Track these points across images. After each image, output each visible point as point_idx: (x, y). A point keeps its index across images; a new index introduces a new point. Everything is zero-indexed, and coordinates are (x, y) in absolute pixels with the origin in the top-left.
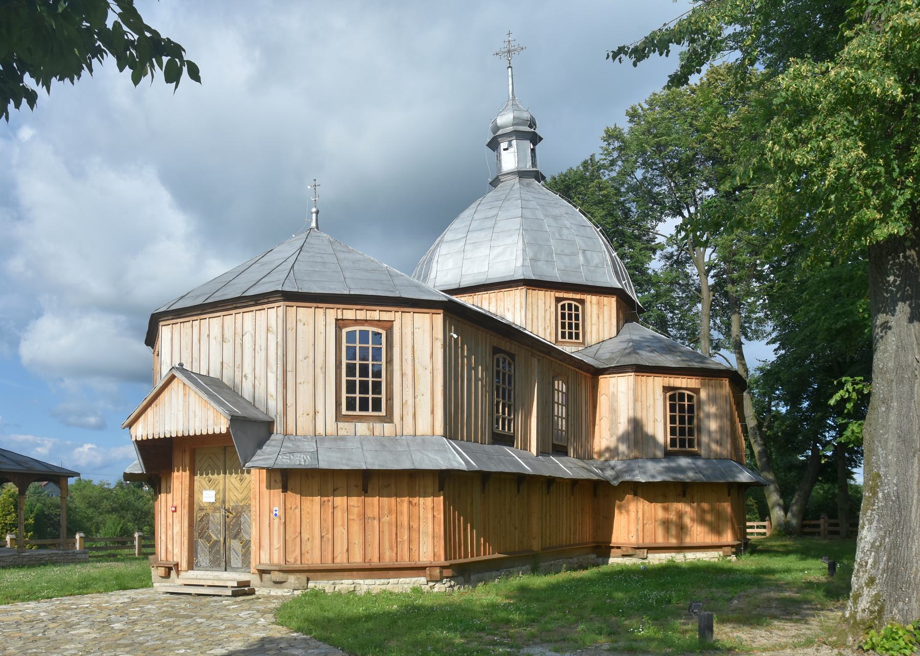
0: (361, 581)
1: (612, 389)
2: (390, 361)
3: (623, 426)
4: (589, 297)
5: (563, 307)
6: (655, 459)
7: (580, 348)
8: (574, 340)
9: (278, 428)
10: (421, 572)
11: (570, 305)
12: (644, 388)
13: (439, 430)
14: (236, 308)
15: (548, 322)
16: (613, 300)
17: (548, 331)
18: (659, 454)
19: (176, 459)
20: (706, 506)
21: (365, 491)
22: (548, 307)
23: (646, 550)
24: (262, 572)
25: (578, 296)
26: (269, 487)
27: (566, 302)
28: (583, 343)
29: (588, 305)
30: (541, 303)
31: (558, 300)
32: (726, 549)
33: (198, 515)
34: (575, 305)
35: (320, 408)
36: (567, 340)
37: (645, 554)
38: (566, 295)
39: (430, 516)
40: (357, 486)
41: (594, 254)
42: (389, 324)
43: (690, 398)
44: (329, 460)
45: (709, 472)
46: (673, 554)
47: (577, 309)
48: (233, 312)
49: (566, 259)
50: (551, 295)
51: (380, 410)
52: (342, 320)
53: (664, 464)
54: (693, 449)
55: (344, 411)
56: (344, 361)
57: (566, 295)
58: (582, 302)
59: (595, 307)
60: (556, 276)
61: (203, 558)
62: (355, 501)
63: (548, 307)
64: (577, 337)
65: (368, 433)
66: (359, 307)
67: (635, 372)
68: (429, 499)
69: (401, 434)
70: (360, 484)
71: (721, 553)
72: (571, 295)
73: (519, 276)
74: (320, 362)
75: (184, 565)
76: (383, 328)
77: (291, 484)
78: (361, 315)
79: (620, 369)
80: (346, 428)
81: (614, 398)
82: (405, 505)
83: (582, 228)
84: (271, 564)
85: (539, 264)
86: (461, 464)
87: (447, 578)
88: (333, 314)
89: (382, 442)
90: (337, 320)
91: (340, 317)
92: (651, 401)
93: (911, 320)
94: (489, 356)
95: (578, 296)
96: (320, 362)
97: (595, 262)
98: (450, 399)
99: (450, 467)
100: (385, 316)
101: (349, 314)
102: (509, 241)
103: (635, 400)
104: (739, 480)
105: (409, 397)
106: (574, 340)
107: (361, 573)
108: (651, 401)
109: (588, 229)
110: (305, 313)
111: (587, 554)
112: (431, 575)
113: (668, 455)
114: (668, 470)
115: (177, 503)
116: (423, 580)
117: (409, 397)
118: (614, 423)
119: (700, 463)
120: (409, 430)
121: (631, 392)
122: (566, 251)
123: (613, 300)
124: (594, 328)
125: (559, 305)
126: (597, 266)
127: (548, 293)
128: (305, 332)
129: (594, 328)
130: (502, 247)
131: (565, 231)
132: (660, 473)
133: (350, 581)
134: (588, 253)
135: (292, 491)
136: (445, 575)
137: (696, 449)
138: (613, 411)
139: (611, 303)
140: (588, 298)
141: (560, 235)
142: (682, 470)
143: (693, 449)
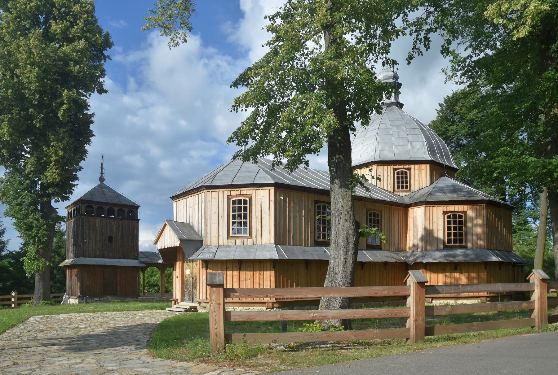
0: (237, 308)
1: (415, 214)
2: (251, 212)
3: (420, 232)
4: (413, 166)
5: (398, 173)
6: (438, 250)
7: (408, 194)
8: (404, 190)
9: (205, 243)
10: (264, 305)
11: (402, 173)
12: (431, 213)
13: (273, 241)
14: (193, 194)
15: (389, 181)
16: (428, 167)
17: (389, 186)
18: (442, 246)
19: (178, 257)
20: (473, 275)
21: (240, 269)
22: (389, 174)
23: (431, 299)
24: (200, 303)
25: (407, 167)
26: (202, 268)
27: (400, 170)
28: (410, 190)
29: (413, 170)
30: (385, 172)
31: (395, 170)
32: (483, 299)
33: (185, 279)
34: (405, 171)
35: (221, 234)
36: (400, 190)
37: (431, 300)
38: (400, 167)
39: (269, 279)
40: (236, 267)
41: (417, 143)
42: (251, 195)
43: (461, 217)
44: (221, 256)
45: (473, 256)
46: (448, 301)
47: (406, 173)
48: (192, 195)
49: (400, 148)
50: (391, 168)
51: (247, 234)
52: (230, 195)
53: (445, 253)
54: (462, 244)
55: (231, 235)
56: (231, 213)
57: (400, 167)
58: (409, 169)
59: (417, 172)
60: (390, 156)
61: (186, 297)
62: (235, 273)
63: (389, 174)
64: (406, 188)
65: (241, 244)
66: (237, 189)
67: (425, 205)
68: (268, 272)
69: (261, 243)
70: (238, 266)
71: (479, 301)
72: (402, 166)
73: (372, 160)
74: (221, 215)
75: (180, 300)
76: (248, 197)
77: (209, 266)
78: (238, 193)
79: (418, 204)
80: (232, 242)
81: (415, 219)
82: (258, 274)
83: (413, 130)
84: (203, 300)
85: (384, 152)
86: (277, 256)
87: (276, 307)
88: (226, 193)
89: (246, 248)
90: (228, 196)
91: (229, 194)
92: (435, 220)
93: (340, 187)
94: (311, 205)
95: (407, 167)
96: (221, 215)
97: (417, 147)
98: (280, 227)
99: (271, 258)
100: (248, 192)
101: (233, 193)
102: (370, 142)
103: (426, 220)
104: (490, 260)
105: (259, 227)
106: (400, 190)
107: (261, 304)
108: (435, 220)
109: (416, 130)
110: (215, 194)
111: (399, 300)
112: (268, 306)
113: (446, 247)
114: (445, 256)
115: (178, 275)
116: (264, 308)
117: (259, 227)
118: (416, 232)
119: (469, 252)
120: (259, 242)
121: (423, 216)
122: (401, 144)
123: (428, 167)
124: (417, 183)
125: (396, 172)
126: (418, 149)
127: (389, 167)
128: (215, 202)
129: (417, 183)
130: (367, 146)
131: (402, 133)
132: (441, 257)
133: (233, 308)
134: (414, 143)
135: (209, 269)
136: (275, 306)
137: (464, 244)
138: (415, 226)
139: (426, 168)
140: (412, 167)
141: (399, 135)
142: (454, 256)
143: (462, 244)
